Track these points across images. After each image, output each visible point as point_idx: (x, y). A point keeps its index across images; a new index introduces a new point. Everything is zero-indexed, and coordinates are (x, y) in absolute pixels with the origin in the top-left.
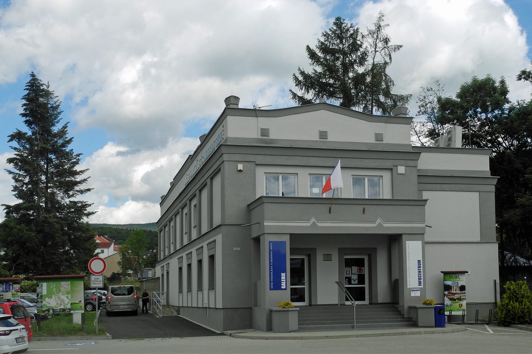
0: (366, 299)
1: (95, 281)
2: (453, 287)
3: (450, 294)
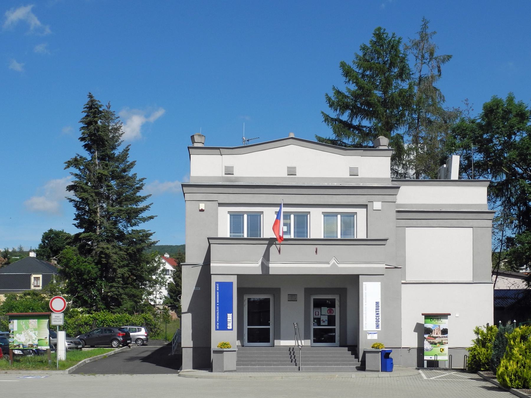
0: (336, 341)
1: (55, 319)
2: (434, 330)
3: (430, 338)
